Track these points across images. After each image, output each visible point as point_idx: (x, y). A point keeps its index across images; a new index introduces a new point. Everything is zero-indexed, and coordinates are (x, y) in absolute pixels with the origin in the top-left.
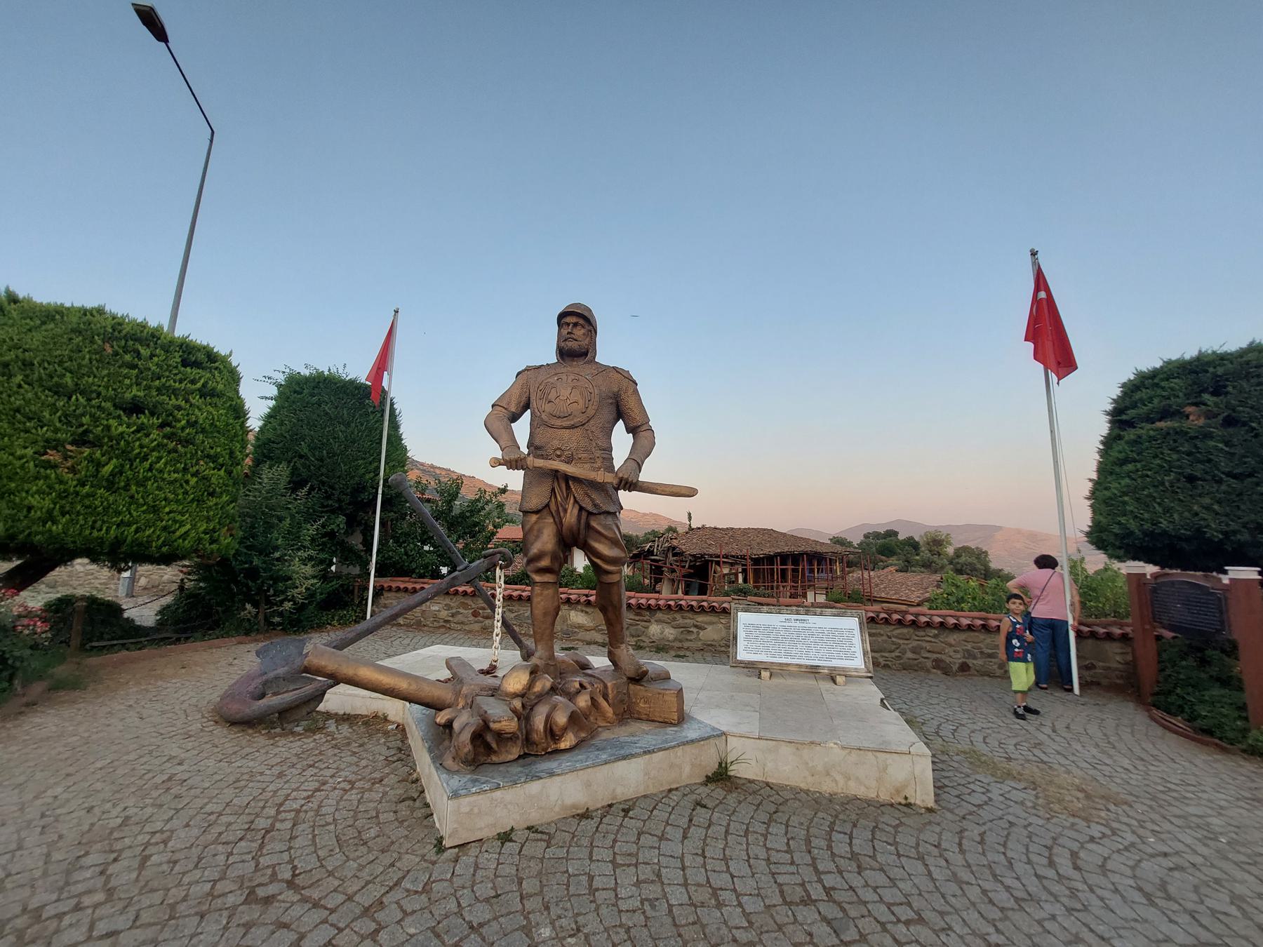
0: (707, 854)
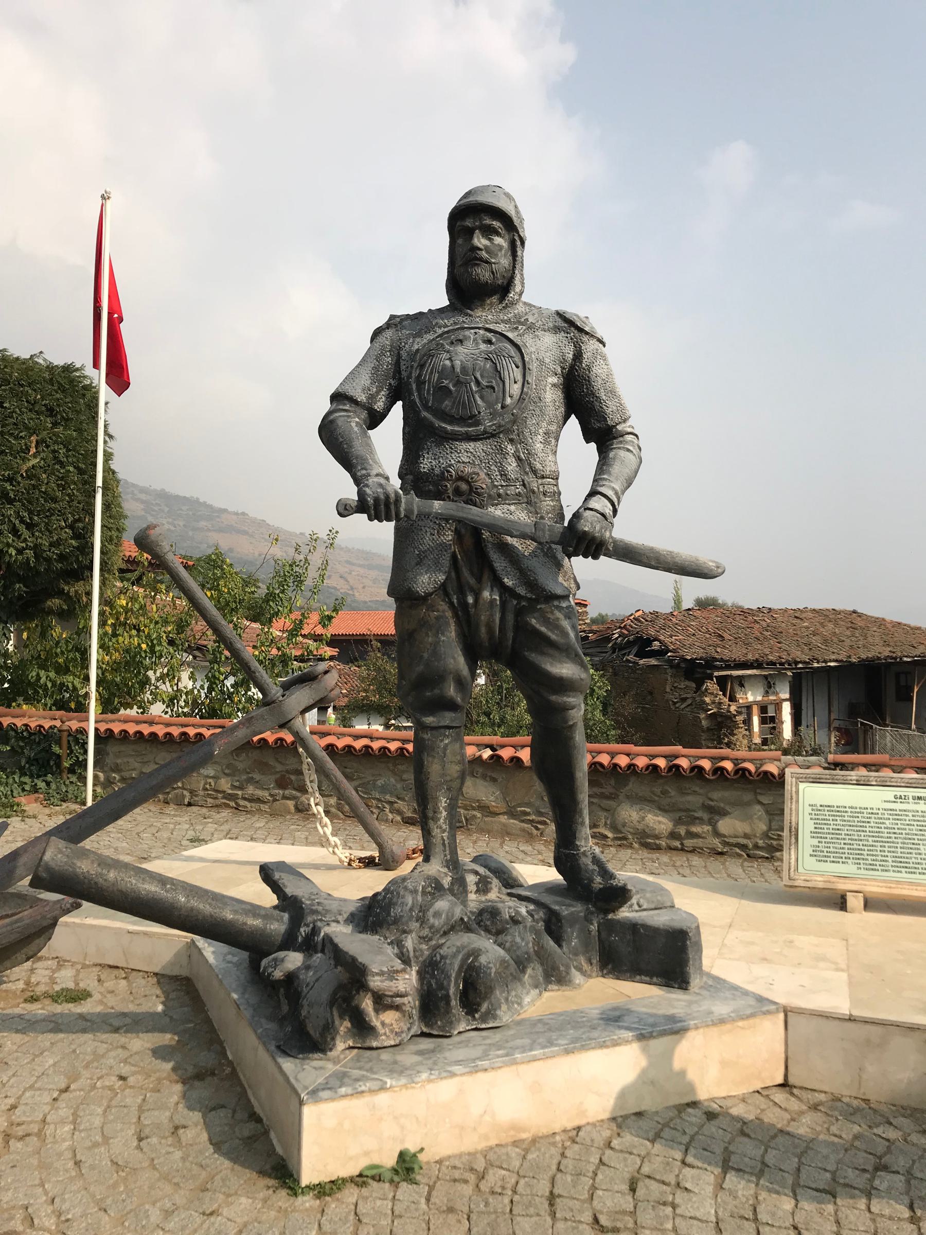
0: (763, 1217)
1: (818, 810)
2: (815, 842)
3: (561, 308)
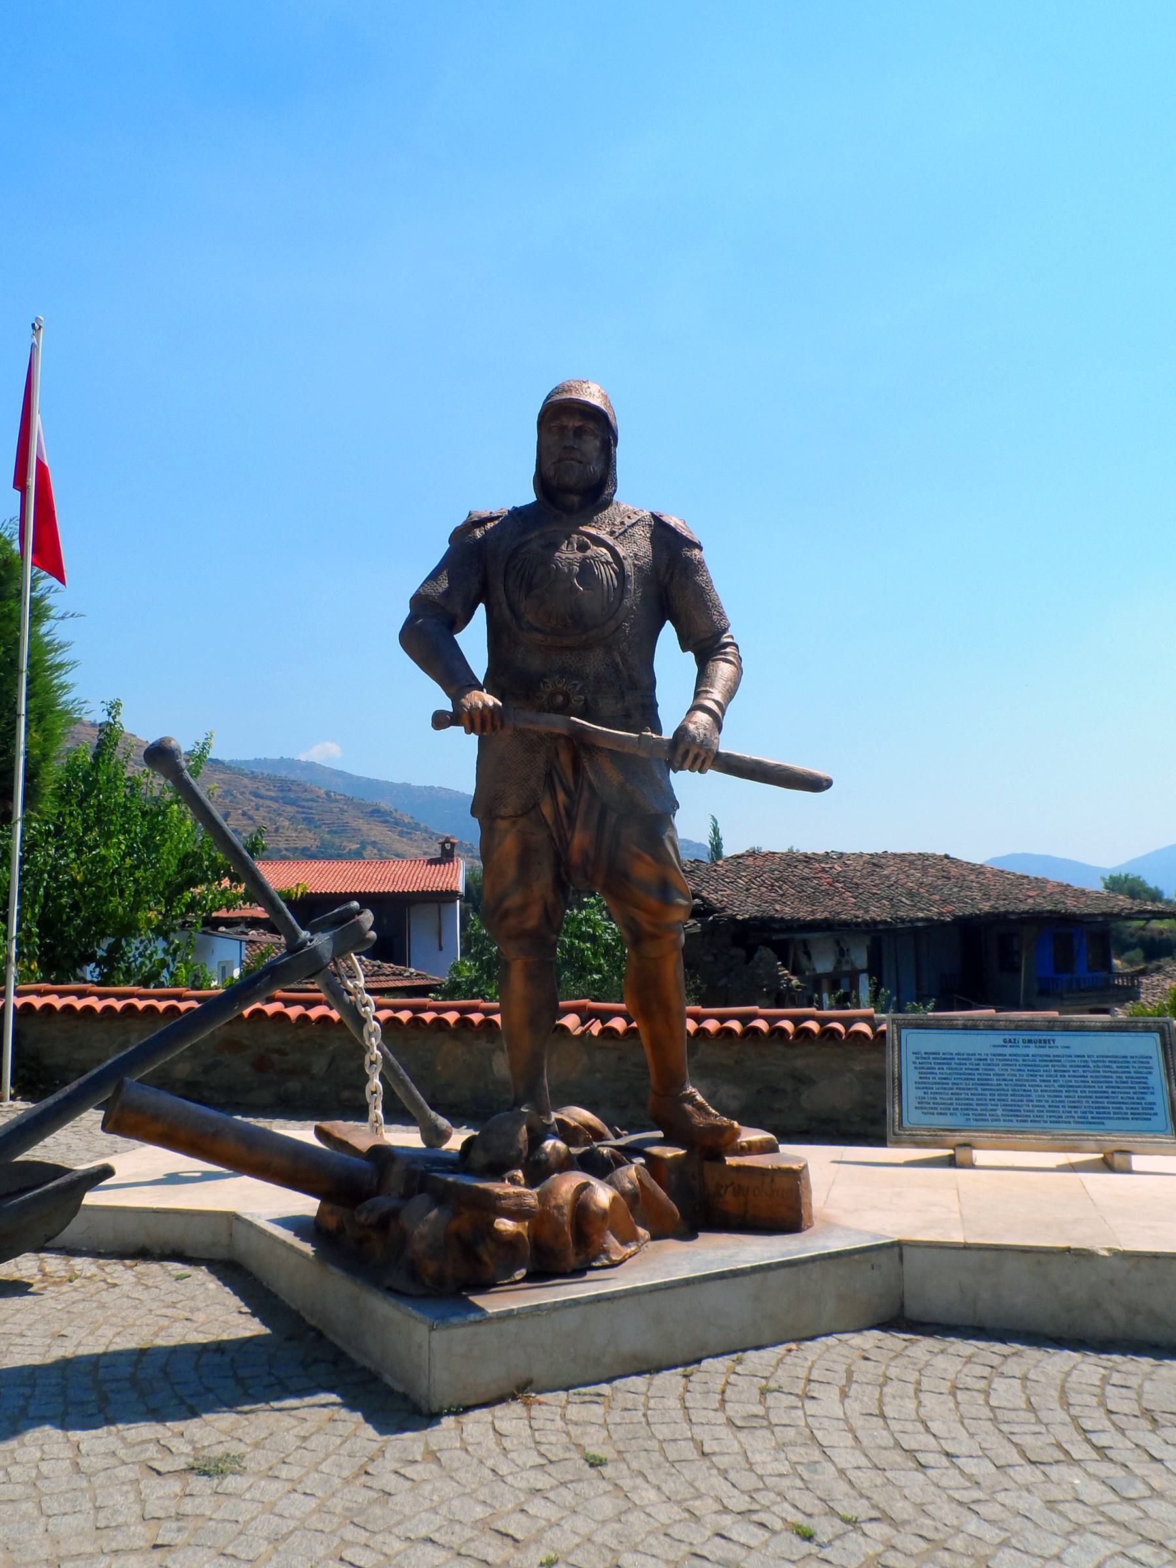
1: (925, 1059)
2: (921, 1093)
3: (657, 510)
